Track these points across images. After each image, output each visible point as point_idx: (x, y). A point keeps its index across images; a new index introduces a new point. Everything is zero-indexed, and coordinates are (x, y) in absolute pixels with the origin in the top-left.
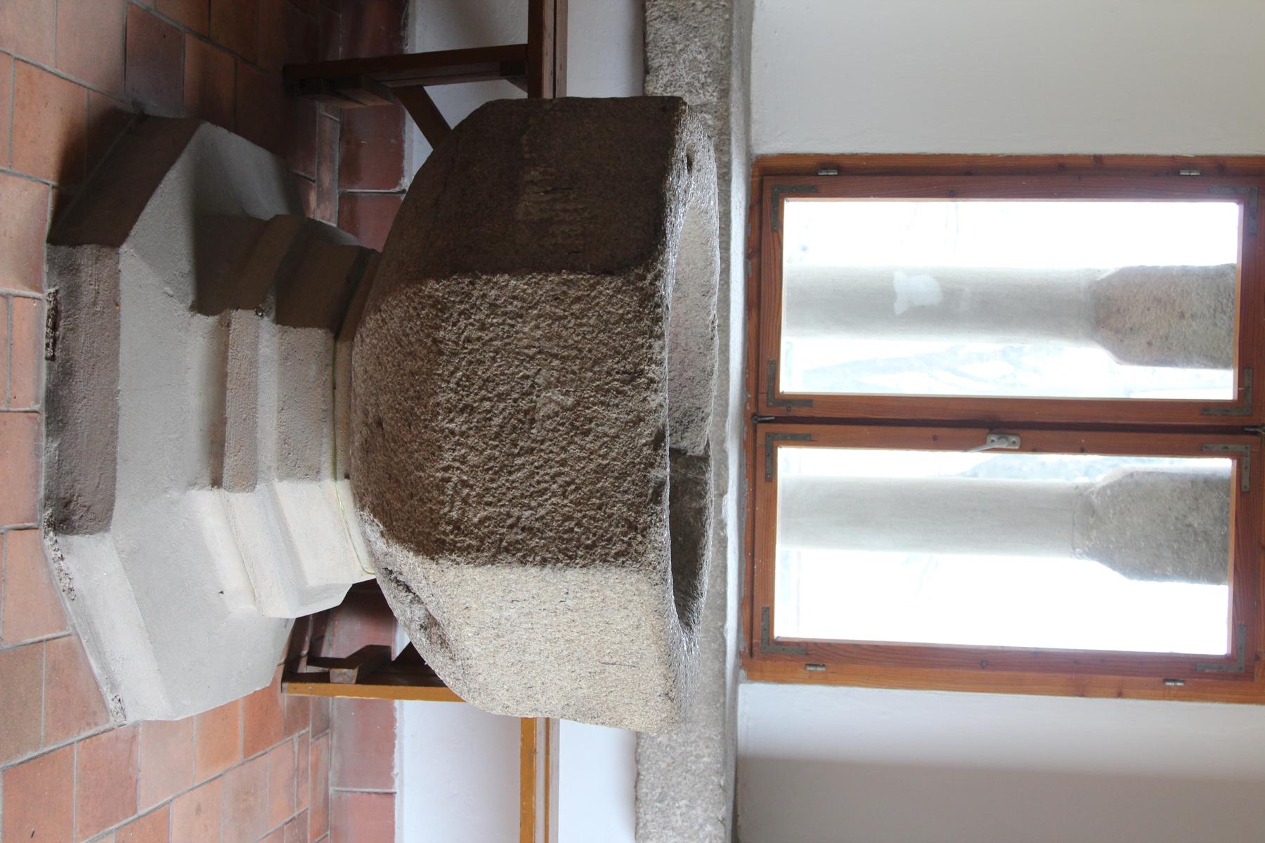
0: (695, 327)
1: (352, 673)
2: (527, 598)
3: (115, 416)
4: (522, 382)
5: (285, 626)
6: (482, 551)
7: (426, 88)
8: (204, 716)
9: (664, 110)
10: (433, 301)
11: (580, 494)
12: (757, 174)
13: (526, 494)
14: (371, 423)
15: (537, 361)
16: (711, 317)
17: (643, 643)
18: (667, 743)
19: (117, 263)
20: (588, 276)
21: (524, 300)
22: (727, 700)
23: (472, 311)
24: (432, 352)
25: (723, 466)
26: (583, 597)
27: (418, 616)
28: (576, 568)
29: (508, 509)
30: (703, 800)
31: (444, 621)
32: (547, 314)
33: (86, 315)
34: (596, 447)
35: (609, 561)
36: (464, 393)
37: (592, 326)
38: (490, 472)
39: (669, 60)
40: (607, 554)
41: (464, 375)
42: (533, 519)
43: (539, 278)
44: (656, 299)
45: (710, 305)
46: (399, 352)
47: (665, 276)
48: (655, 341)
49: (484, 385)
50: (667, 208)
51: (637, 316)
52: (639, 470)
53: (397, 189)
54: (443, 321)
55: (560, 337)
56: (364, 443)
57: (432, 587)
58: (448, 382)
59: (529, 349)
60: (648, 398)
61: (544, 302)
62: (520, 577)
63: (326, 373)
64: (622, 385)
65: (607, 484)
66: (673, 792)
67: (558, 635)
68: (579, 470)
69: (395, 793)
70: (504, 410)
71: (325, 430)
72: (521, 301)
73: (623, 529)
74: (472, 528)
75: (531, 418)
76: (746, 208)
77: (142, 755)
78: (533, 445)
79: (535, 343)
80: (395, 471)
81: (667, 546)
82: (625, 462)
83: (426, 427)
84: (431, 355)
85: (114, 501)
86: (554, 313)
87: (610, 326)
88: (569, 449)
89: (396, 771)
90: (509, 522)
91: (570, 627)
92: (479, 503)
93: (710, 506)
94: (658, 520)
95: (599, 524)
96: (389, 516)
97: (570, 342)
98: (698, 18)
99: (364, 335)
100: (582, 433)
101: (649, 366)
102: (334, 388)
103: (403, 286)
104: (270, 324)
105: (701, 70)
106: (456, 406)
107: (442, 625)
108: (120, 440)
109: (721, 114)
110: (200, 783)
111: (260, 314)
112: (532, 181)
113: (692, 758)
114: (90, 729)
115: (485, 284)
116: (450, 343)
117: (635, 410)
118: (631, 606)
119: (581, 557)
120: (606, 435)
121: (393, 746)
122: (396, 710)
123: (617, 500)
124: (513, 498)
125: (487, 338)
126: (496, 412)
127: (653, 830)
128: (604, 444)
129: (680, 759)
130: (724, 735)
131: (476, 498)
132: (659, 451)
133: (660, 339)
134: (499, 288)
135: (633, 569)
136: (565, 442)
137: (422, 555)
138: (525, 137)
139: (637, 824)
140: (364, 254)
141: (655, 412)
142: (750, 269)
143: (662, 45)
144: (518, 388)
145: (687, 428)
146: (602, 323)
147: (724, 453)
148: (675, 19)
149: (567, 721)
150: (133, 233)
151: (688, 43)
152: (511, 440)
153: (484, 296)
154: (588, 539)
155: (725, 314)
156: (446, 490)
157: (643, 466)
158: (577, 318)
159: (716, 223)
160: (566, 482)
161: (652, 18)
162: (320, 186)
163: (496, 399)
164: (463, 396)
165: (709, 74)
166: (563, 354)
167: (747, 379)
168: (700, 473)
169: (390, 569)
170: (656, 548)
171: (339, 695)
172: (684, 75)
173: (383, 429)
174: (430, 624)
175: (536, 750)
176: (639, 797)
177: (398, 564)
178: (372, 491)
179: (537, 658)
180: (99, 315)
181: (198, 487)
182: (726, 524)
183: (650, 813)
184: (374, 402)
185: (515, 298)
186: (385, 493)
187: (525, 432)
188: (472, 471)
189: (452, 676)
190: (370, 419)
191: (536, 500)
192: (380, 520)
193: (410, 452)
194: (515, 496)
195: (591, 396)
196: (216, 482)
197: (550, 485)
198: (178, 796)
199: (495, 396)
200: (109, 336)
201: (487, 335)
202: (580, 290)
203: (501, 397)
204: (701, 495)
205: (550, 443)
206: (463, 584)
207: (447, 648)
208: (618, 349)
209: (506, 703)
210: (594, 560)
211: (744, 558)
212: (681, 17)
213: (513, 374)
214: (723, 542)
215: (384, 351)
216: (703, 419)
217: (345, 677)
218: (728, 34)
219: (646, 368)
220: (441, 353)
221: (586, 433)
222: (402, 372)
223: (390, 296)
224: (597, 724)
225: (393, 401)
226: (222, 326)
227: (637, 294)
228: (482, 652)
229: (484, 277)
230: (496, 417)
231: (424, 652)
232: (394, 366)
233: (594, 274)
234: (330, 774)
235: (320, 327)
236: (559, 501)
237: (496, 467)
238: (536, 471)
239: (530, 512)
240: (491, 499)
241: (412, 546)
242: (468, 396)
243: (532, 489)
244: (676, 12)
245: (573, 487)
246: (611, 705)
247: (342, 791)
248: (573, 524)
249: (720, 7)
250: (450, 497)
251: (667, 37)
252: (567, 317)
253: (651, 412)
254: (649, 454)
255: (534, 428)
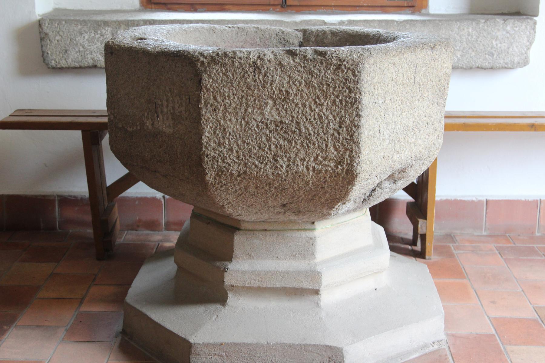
0: (232, 37)
1: (421, 222)
2: (378, 125)
3: (281, 345)
4: (260, 128)
5: (395, 257)
6: (352, 149)
7: (108, 185)
8: (442, 300)
9: (112, 53)
10: (217, 176)
11: (321, 96)
12: (150, 6)
13: (321, 126)
14: (284, 210)
15: (249, 120)
16: (227, 28)
17: (403, 61)
18: (461, 52)
19: (200, 344)
20: (202, 92)
21: (216, 128)
22: (437, 19)
23: (222, 156)
24: (245, 177)
25: (309, 23)
26: (378, 94)
27: (388, 185)
28: (361, 98)
29: (330, 135)
30: (493, 31)
31: (391, 171)
32: (223, 115)
33: (227, 360)
34: (295, 87)
35: (358, 80)
36: (267, 159)
37: (229, 90)
38: (309, 145)
39: (89, 54)
40: (354, 81)
41: (257, 160)
42: (335, 121)
43: (203, 120)
44: (214, 55)
45: (220, 29)
46: (245, 195)
47: (202, 51)
48: (237, 55)
49: (262, 149)
50: (165, 50)
51: (223, 66)
52: (308, 64)
53: (163, 200)
54: (228, 171)
55: (235, 108)
56: (295, 214)
57: (372, 177)
58: (261, 168)
59: (242, 125)
60: (268, 59)
61: (217, 117)
62: (366, 129)
63: (258, 234)
64: (261, 73)
65: (315, 81)
66: (488, 48)
67: (399, 108)
68: (308, 97)
69: (486, 199)
70: (275, 138)
71: (288, 235)
72: (216, 129)
73: (340, 72)
74: (340, 155)
75: (280, 123)
76: (169, 12)
77: (463, 331)
78: (294, 122)
79: (239, 121)
80: (310, 197)
81: (349, 48)
82: (303, 71)
83: (285, 180)
84: (247, 177)
85: (326, 346)
86: (223, 111)
87: (229, 80)
88: (296, 102)
89: (474, 199)
90: (336, 135)
91: (394, 102)
92: (326, 151)
93: (330, 28)
94: (335, 53)
95: (337, 86)
96: (333, 200)
97: (238, 102)
98: (65, 39)
99: (237, 214)
100: (288, 95)
101: (250, 59)
102: (266, 230)
103: (210, 193)
104: (231, 265)
105: (94, 37)
106: (274, 164)
107: (393, 171)
108: (294, 342)
109: (117, 25)
110: (479, 302)
111: (226, 270)
112: (152, 124)
113: (469, 38)
114: (448, 358)
115: (207, 149)
116: (240, 167)
117: (275, 66)
118: (382, 68)
119: (355, 95)
120: (289, 82)
121: (461, 201)
122: (442, 199)
123: (324, 76)
124: (324, 133)
125: (237, 148)
126: (277, 142)
127: (509, 59)
128: (293, 83)
129: (470, 45)
130: (457, 21)
131: (324, 153)
132: (297, 53)
133: (236, 53)
134: (209, 141)
135: (362, 67)
136: (293, 104)
137: (354, 182)
138: (129, 129)
139: (506, 68)
140: (195, 216)
141: (276, 55)
142: (202, 9)
143: (81, 58)
144: (264, 130)
145: (287, 41)
146: (227, 85)
147: (302, 22)
148: (66, 51)
149: (446, 104)
150: (184, 336)
151: (79, 44)
152: (292, 134)
153: (214, 149)
154: (345, 91)
155: (226, 22)
156: (319, 169)
157: (305, 62)
158: (225, 98)
159: (174, 26)
160: (314, 104)
161: (66, 64)
162: (161, 241)
163: (270, 142)
164: (268, 160)
165: (96, 32)
166: (245, 106)
167: (262, 11)
168: (312, 34)
169: (363, 200)
170: (351, 54)
171: (432, 229)
172: (96, 46)
173: (287, 204)
174: (393, 178)
175: (463, 123)
176: (490, 67)
177: (360, 195)
178: (321, 209)
179: (411, 120)
180: (228, 354)
181: (319, 302)
182: (341, 21)
183: (499, 61)
184: (273, 208)
185: (215, 133)
186: (321, 202)
187: (287, 126)
188: (309, 155)
189: (421, 166)
190: (282, 211)
191: (324, 120)
192: (336, 205)
193: (299, 189)
194: (322, 131)
195: (268, 91)
196: (316, 292)
197: (316, 112)
198: (486, 313)
199: (268, 143)
200: (239, 349)
201: (235, 148)
202: (210, 97)
203: (269, 139)
204: (324, 33)
205: (293, 113)
206: (370, 160)
207: (405, 169)
208: (242, 76)
209: (436, 137)
210: (357, 88)
211: (360, 11)
212: (65, 48)
213: (256, 133)
214: (351, 22)
215: (245, 203)
216: (283, 33)
217: (423, 225)
218: (73, 22)
219: (252, 60)
220: (245, 172)
221: (288, 93)
222: (256, 194)
223: (215, 200)
224: (448, 87)
225: (272, 198)
226: (233, 290)
227: (211, 65)
228: (408, 149)
229: (204, 149)
230: (279, 143)
231: (408, 181)
232: (253, 198)
233: (201, 90)
234: (476, 234)
235: (233, 238)
236: (325, 107)
237: (306, 142)
238: (308, 120)
239: (331, 123)
240: (324, 145)
241: (350, 187)
242: (268, 158)
243: (319, 122)
244: (62, 51)
245: (317, 100)
246: (438, 79)
247: (485, 227)
248: (337, 100)
249: (59, 26)
250: (323, 167)
251: (76, 56)
252: (224, 104)
253: (276, 58)
254: (299, 58)
255: (285, 122)
